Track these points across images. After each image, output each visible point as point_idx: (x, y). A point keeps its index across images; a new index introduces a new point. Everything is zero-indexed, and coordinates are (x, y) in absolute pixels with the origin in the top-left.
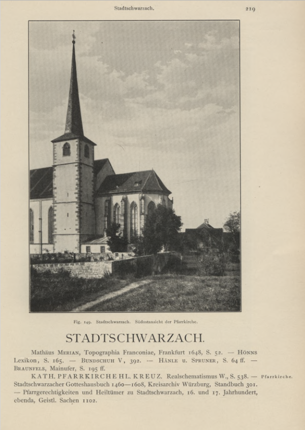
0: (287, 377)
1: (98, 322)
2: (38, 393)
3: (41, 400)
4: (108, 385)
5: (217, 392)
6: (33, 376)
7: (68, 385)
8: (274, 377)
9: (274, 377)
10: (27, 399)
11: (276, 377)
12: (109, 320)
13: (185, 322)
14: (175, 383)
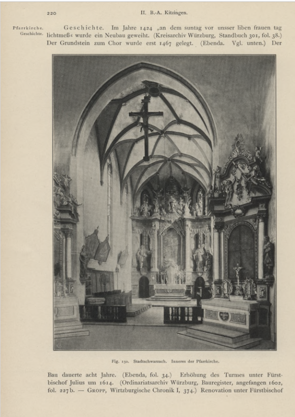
1: (135, 361)
3: (62, 43)
5: (170, 43)
7: (90, 391)
9: (25, 29)
10: (74, 41)
12: (146, 360)
14: (181, 34)
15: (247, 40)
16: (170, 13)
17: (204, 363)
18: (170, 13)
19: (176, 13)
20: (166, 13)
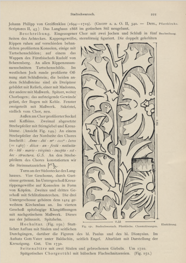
0: (175, 24)
2: (47, 127)
4: (64, 176)
8: (167, 24)
9: (167, 24)
11: (168, 24)
13: (125, 227)
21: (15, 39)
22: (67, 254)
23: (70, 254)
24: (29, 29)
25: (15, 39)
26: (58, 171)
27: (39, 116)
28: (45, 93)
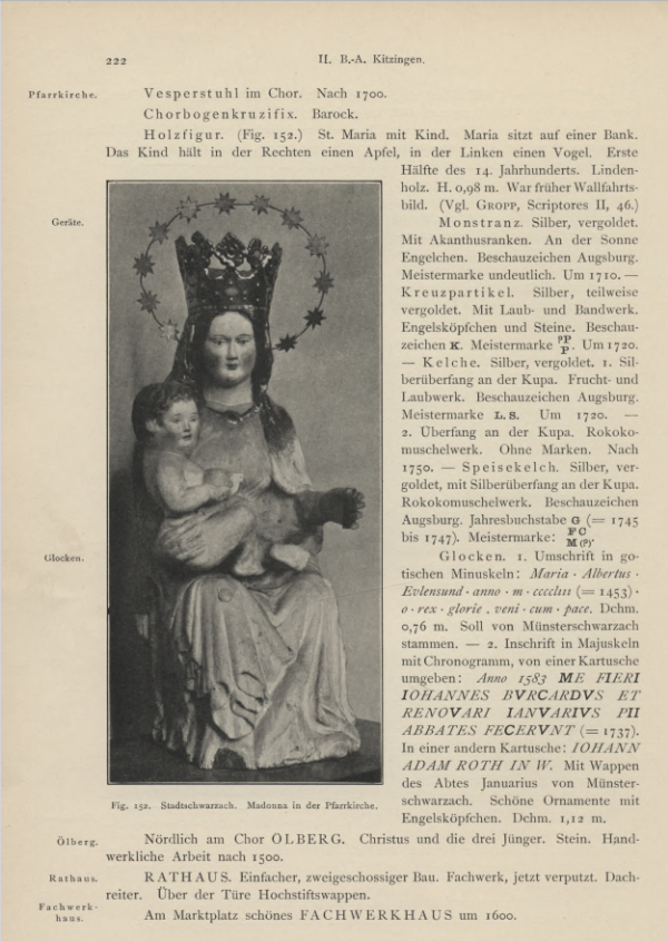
0: (84, 95)
1: (164, 806)
6: (418, 135)
7: (336, 841)
8: (57, 96)
9: (57, 96)
11: (60, 96)
13: (349, 807)
15: (531, 320)
16: (385, 60)
17: (343, 810)
18: (385, 60)
19: (400, 60)
20: (375, 59)
21: (425, 574)
22: (224, 94)
23: (234, 94)
24: (601, 205)
25: (425, 574)
26: (476, 276)
27: (429, 661)
28: (622, 315)
